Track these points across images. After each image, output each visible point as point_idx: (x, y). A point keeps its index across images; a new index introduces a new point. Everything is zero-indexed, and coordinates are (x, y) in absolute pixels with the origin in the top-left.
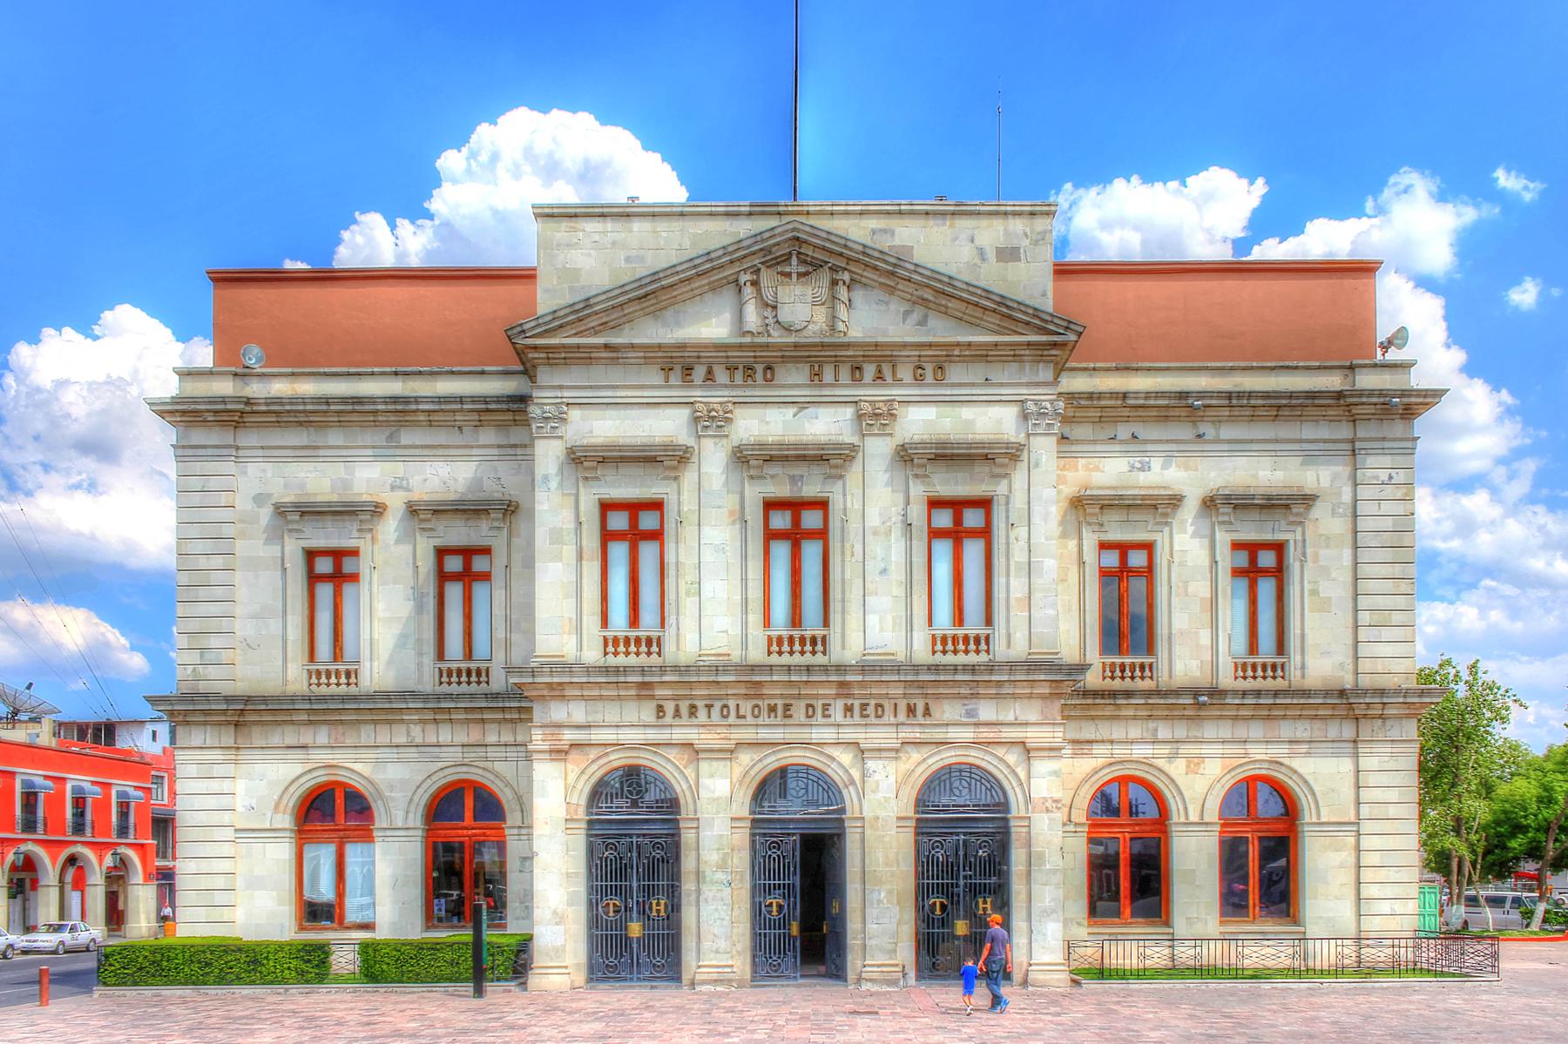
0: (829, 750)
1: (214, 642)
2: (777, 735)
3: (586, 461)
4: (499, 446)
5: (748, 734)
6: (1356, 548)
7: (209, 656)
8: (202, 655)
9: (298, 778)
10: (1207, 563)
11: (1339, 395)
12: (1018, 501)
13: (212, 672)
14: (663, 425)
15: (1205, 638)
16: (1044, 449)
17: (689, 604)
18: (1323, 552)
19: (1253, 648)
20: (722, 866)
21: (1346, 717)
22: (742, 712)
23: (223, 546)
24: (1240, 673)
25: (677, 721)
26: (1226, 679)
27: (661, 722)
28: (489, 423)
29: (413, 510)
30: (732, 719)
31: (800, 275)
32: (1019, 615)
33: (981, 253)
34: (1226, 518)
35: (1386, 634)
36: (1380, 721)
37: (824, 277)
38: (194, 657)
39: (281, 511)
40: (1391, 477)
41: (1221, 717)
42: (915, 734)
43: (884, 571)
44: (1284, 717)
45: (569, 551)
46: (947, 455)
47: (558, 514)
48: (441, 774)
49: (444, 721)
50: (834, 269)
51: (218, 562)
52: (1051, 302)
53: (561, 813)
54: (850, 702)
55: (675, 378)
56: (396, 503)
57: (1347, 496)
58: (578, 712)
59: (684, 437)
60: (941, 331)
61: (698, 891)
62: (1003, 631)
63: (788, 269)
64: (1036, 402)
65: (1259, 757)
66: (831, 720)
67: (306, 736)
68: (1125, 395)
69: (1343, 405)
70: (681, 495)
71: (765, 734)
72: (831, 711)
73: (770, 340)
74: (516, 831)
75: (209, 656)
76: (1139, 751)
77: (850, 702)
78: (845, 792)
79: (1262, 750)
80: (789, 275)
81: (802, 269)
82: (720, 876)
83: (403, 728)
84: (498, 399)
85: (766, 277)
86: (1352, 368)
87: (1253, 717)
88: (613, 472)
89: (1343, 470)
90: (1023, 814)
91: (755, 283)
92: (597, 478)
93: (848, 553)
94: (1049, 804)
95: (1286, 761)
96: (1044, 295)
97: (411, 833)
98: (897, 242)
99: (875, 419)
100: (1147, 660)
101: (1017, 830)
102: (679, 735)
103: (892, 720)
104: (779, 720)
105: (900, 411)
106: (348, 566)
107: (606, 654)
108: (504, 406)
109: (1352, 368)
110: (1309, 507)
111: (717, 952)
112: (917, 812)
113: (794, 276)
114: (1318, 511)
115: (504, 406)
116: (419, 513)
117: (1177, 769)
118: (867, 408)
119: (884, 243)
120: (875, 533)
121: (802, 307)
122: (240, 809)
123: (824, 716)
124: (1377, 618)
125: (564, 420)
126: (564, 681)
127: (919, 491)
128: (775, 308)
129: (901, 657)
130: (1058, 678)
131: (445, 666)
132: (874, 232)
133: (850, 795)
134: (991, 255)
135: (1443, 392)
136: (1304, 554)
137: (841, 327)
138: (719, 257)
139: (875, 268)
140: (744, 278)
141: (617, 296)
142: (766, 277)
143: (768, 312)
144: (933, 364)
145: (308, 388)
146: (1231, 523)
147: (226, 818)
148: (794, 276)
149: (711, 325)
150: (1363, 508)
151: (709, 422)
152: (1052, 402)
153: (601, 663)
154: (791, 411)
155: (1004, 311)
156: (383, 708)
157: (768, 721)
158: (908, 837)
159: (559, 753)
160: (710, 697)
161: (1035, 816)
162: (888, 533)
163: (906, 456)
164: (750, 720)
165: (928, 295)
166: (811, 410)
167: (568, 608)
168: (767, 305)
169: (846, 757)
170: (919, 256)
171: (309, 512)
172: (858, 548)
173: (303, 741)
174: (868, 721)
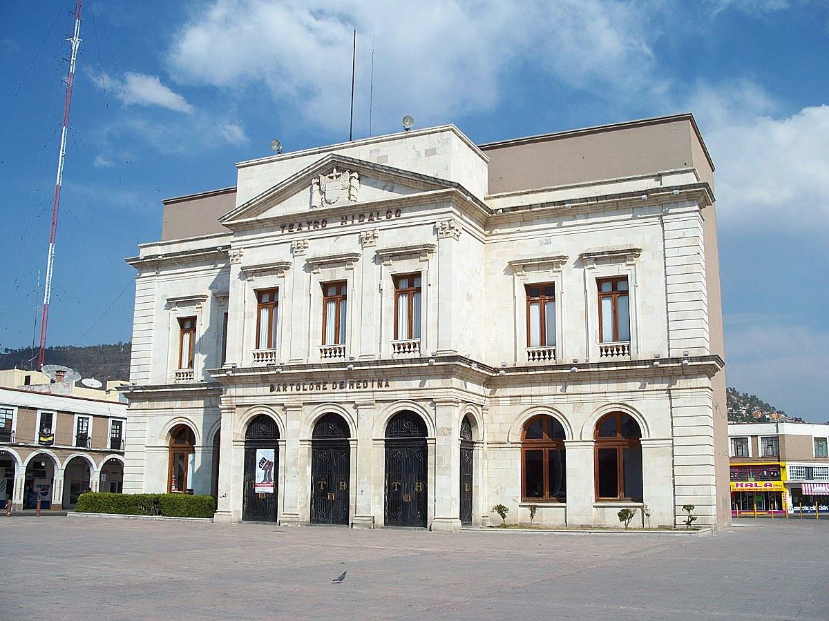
3: (247, 273)
5: (308, 399)
20: (295, 464)
27: (273, 393)
31: (337, 177)
35: (686, 324)
40: (684, 234)
47: (242, 297)
48: (603, 409)
55: (286, 231)
58: (240, 391)
63: (331, 175)
76: (546, 400)
80: (332, 178)
82: (293, 469)
86: (660, 175)
94: (445, 431)
97: (209, 448)
100: (626, 344)
102: (279, 400)
103: (372, 389)
106: (621, 287)
109: (660, 175)
111: (291, 507)
112: (313, 437)
113: (335, 178)
116: (586, 259)
124: (680, 316)
131: (530, 350)
134: (423, 154)
144: (393, 209)
148: (335, 178)
149: (298, 204)
156: (578, 373)
158: (381, 450)
171: (527, 265)
174: (360, 390)
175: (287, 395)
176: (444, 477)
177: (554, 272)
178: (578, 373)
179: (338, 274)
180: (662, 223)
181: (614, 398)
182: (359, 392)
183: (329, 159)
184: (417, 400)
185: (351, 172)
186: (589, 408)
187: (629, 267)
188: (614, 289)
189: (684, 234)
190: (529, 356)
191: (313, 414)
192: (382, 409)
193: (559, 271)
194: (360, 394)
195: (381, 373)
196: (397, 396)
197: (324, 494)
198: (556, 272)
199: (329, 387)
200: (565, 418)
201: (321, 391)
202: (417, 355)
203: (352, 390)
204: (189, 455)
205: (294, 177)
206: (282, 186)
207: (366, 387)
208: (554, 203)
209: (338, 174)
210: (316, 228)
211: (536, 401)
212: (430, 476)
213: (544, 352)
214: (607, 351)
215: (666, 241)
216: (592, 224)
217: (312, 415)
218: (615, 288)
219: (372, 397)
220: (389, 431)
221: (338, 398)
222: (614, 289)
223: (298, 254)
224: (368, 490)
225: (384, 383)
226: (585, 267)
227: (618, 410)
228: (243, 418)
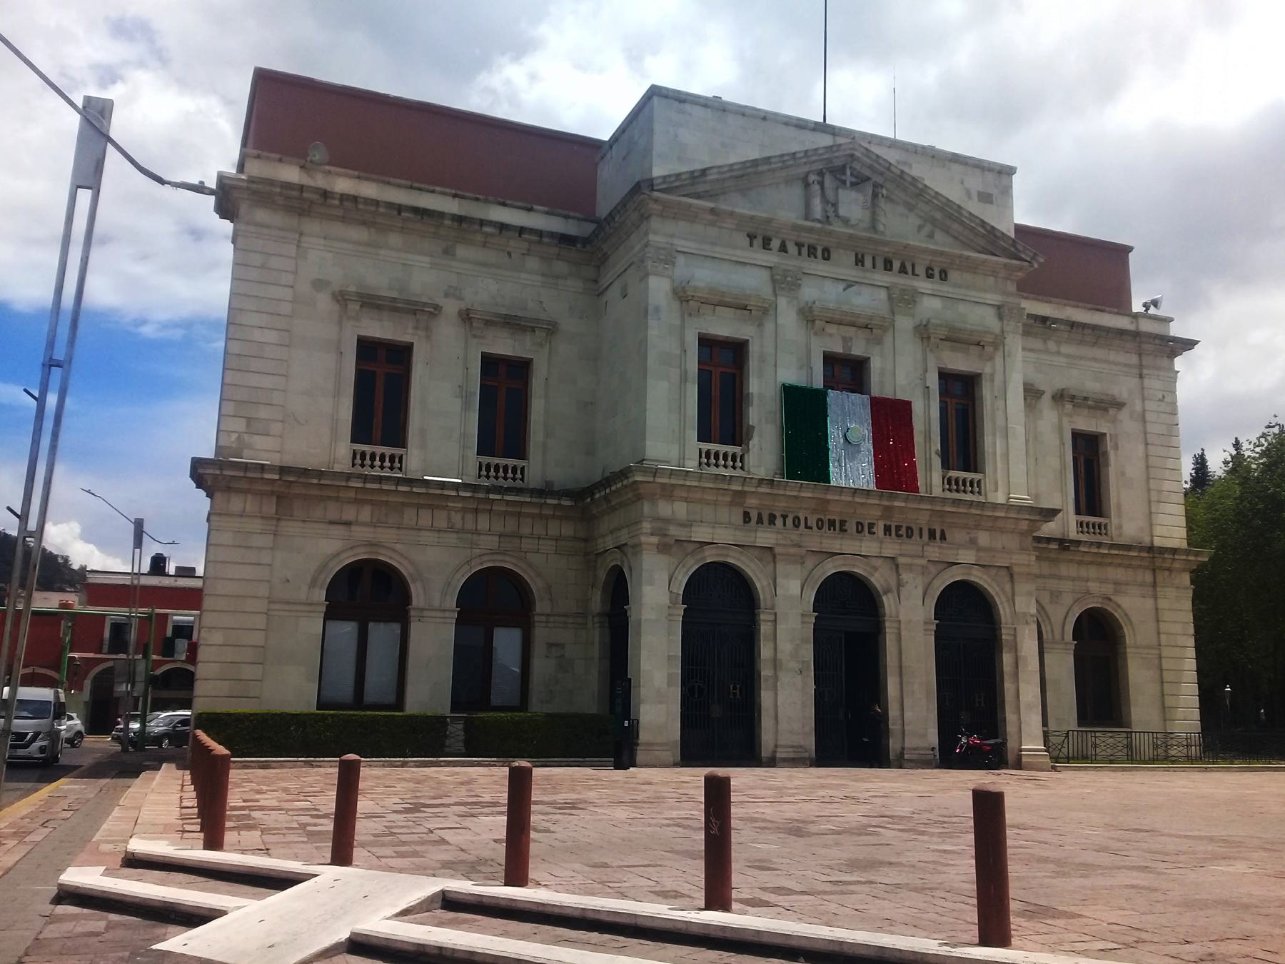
6: (1147, 444)
8: (248, 425)
10: (1058, 443)
13: (259, 442)
14: (751, 280)
16: (1015, 343)
21: (1147, 568)
29: (466, 317)
36: (1167, 573)
39: (341, 298)
41: (1071, 561)
44: (1110, 564)
46: (957, 338)
49: (484, 511)
50: (876, 186)
53: (665, 600)
58: (680, 509)
61: (776, 678)
67: (349, 513)
74: (543, 619)
81: (854, 180)
83: (444, 514)
84: (552, 235)
87: (1091, 563)
97: (447, 614)
107: (700, 464)
114: (1124, 415)
130: (1032, 518)
133: (888, 602)
137: (881, 228)
140: (812, 178)
143: (829, 208)
145: (369, 190)
150: (1149, 417)
151: (784, 282)
163: (923, 332)
165: (938, 216)
168: (828, 202)
173: (345, 517)
180: (1141, 376)
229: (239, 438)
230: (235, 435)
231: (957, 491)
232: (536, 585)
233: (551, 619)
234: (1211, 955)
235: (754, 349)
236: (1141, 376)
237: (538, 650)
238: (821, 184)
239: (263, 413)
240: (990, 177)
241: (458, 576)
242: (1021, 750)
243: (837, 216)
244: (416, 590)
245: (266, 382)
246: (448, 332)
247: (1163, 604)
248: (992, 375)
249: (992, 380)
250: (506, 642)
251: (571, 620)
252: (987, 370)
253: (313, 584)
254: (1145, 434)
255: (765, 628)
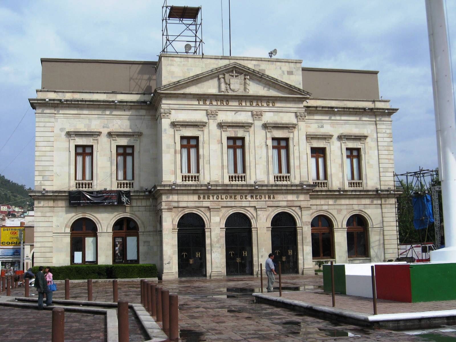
0: (247, 208)
1: (47, 173)
2: (233, 204)
4: (136, 116)
5: (225, 204)
7: (46, 178)
8: (43, 178)
9: (73, 217)
11: (372, 109)
12: (296, 139)
13: (47, 183)
15: (340, 175)
17: (207, 166)
18: (370, 151)
19: (353, 178)
20: (218, 242)
22: (222, 198)
23: (50, 144)
24: (350, 185)
25: (204, 200)
26: (347, 187)
28: (134, 109)
30: (220, 200)
32: (297, 171)
33: (283, 72)
34: (344, 142)
37: (242, 77)
38: (40, 178)
40: (386, 131)
42: (270, 204)
43: (261, 158)
45: (172, 151)
47: (170, 140)
51: (48, 149)
52: (302, 86)
53: (171, 227)
54: (252, 195)
55: (201, 103)
56: (105, 131)
57: (375, 136)
58: (175, 198)
59: (205, 119)
60: (273, 93)
62: (293, 175)
63: (233, 74)
64: (300, 113)
65: (356, 209)
66: (248, 200)
68: (316, 107)
69: (373, 112)
70: (203, 136)
71: (229, 204)
72: (237, 197)
73: (229, 94)
75: (46, 178)
76: (325, 208)
77: (252, 195)
78: (252, 221)
79: (356, 206)
80: (233, 76)
82: (217, 245)
85: (227, 76)
88: (185, 129)
89: (373, 127)
90: (300, 226)
91: (224, 78)
92: (180, 130)
93: (251, 153)
95: (364, 210)
96: (300, 84)
98: (261, 68)
99: (257, 115)
101: (299, 231)
102: (206, 204)
103: (264, 200)
104: (233, 200)
105: (263, 114)
108: (140, 104)
110: (365, 139)
113: (234, 76)
114: (368, 140)
115: (140, 104)
117: (334, 213)
118: (255, 113)
119: (257, 69)
120: (258, 147)
121: (236, 85)
122: (54, 226)
123: (245, 199)
125: (170, 114)
126: (173, 190)
127: (269, 135)
128: (229, 85)
129: (266, 183)
132: (255, 65)
133: (253, 221)
134: (286, 73)
135: (397, 110)
136: (365, 152)
138: (215, 71)
139: (256, 75)
140: (221, 76)
141: (187, 80)
142: (227, 76)
144: (271, 100)
146: (346, 143)
147: (50, 229)
148: (234, 76)
149: (210, 87)
150: (379, 139)
151: (211, 115)
152: (304, 113)
153: (182, 183)
154: (234, 113)
155: (290, 89)
156: (339, 194)
157: (230, 200)
158: (270, 233)
159: (170, 209)
160: (213, 193)
161: (304, 227)
162: (261, 147)
163: (265, 126)
164: (225, 200)
166: (239, 113)
167: (172, 167)
169: (252, 210)
170: (267, 73)
172: (253, 151)
175: (211, 201)
176: (308, 247)
177: (326, 143)
178: (339, 194)
179: (240, 133)
180: (376, 124)
181: (356, 207)
182: (257, 201)
183: (233, 65)
184: (290, 206)
185: (245, 75)
186: (344, 212)
187: (327, 144)
188: (355, 154)
189: (386, 131)
190: (349, 184)
191: (228, 213)
192: (270, 211)
193: (329, 143)
194: (258, 202)
195: (271, 191)
196: (295, 204)
197: (234, 259)
198: (327, 142)
199: (238, 197)
200: (334, 217)
201: (233, 200)
202: (289, 183)
203: (231, 200)
204: (87, 239)
205: (206, 73)
206: (202, 75)
207: (261, 199)
208: (329, 107)
209: (237, 75)
210: (222, 104)
211: (319, 208)
212: (300, 247)
213: (127, 184)
214: (121, 185)
215: (378, 134)
216: (63, 114)
217: (227, 214)
218: (84, 150)
219: (265, 204)
220: (227, 224)
221: (244, 204)
222: (355, 154)
223: (212, 118)
224: (216, 259)
225: (272, 197)
226: (70, 138)
227: (358, 213)
228: (179, 215)
229: (40, 183)
230: (39, 182)
231: (280, 181)
232: (139, 223)
233: (145, 233)
234: (238, 319)
235: (201, 139)
236: (376, 124)
237: (141, 244)
238: (224, 78)
239: (47, 173)
240: (292, 65)
241: (112, 221)
242: (304, 269)
243: (230, 89)
244: (98, 226)
245: (47, 163)
246: (104, 140)
247: (384, 211)
248: (293, 138)
249: (293, 140)
250: (131, 241)
251: (152, 233)
252: (291, 136)
253: (66, 226)
254: (378, 146)
255: (207, 234)
